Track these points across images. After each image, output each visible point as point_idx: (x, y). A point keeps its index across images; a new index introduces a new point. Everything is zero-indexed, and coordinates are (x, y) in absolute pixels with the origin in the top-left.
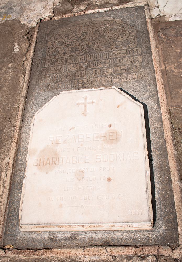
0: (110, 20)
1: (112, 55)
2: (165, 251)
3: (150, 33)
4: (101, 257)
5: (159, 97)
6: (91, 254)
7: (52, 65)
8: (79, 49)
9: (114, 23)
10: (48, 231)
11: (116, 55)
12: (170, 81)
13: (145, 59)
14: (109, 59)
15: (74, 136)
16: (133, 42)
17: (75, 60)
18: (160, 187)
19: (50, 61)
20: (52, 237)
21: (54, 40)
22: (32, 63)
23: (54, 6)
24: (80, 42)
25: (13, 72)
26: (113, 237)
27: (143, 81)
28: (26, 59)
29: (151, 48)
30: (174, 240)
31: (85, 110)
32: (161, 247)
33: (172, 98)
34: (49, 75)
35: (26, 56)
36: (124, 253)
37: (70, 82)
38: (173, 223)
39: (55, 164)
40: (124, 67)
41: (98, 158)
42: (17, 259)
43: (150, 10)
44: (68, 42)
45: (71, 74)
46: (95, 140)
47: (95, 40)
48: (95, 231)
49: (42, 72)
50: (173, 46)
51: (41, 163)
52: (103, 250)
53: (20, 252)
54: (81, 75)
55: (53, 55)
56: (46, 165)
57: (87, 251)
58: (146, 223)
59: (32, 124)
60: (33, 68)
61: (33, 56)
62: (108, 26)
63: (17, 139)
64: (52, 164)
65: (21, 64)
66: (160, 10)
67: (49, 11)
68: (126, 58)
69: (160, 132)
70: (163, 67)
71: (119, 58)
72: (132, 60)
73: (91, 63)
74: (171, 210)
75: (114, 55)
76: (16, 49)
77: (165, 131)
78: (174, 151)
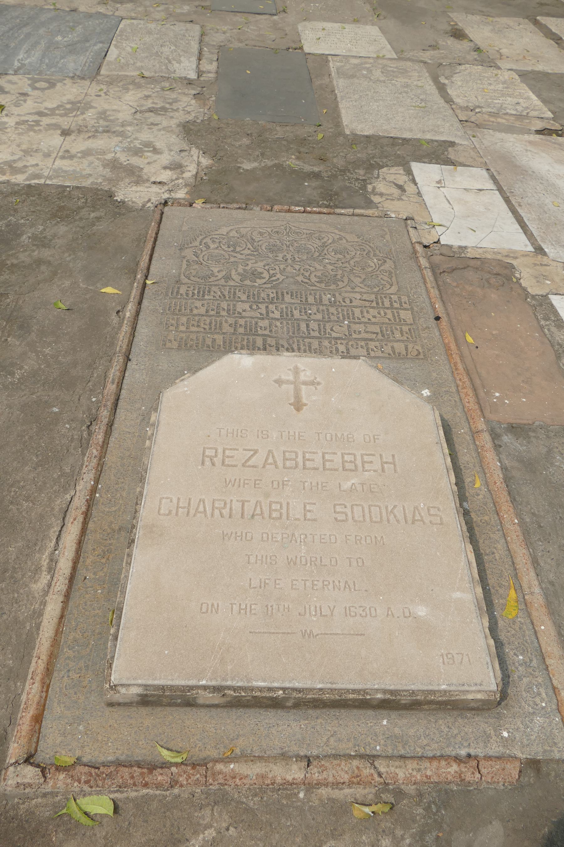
69: (240, 167)
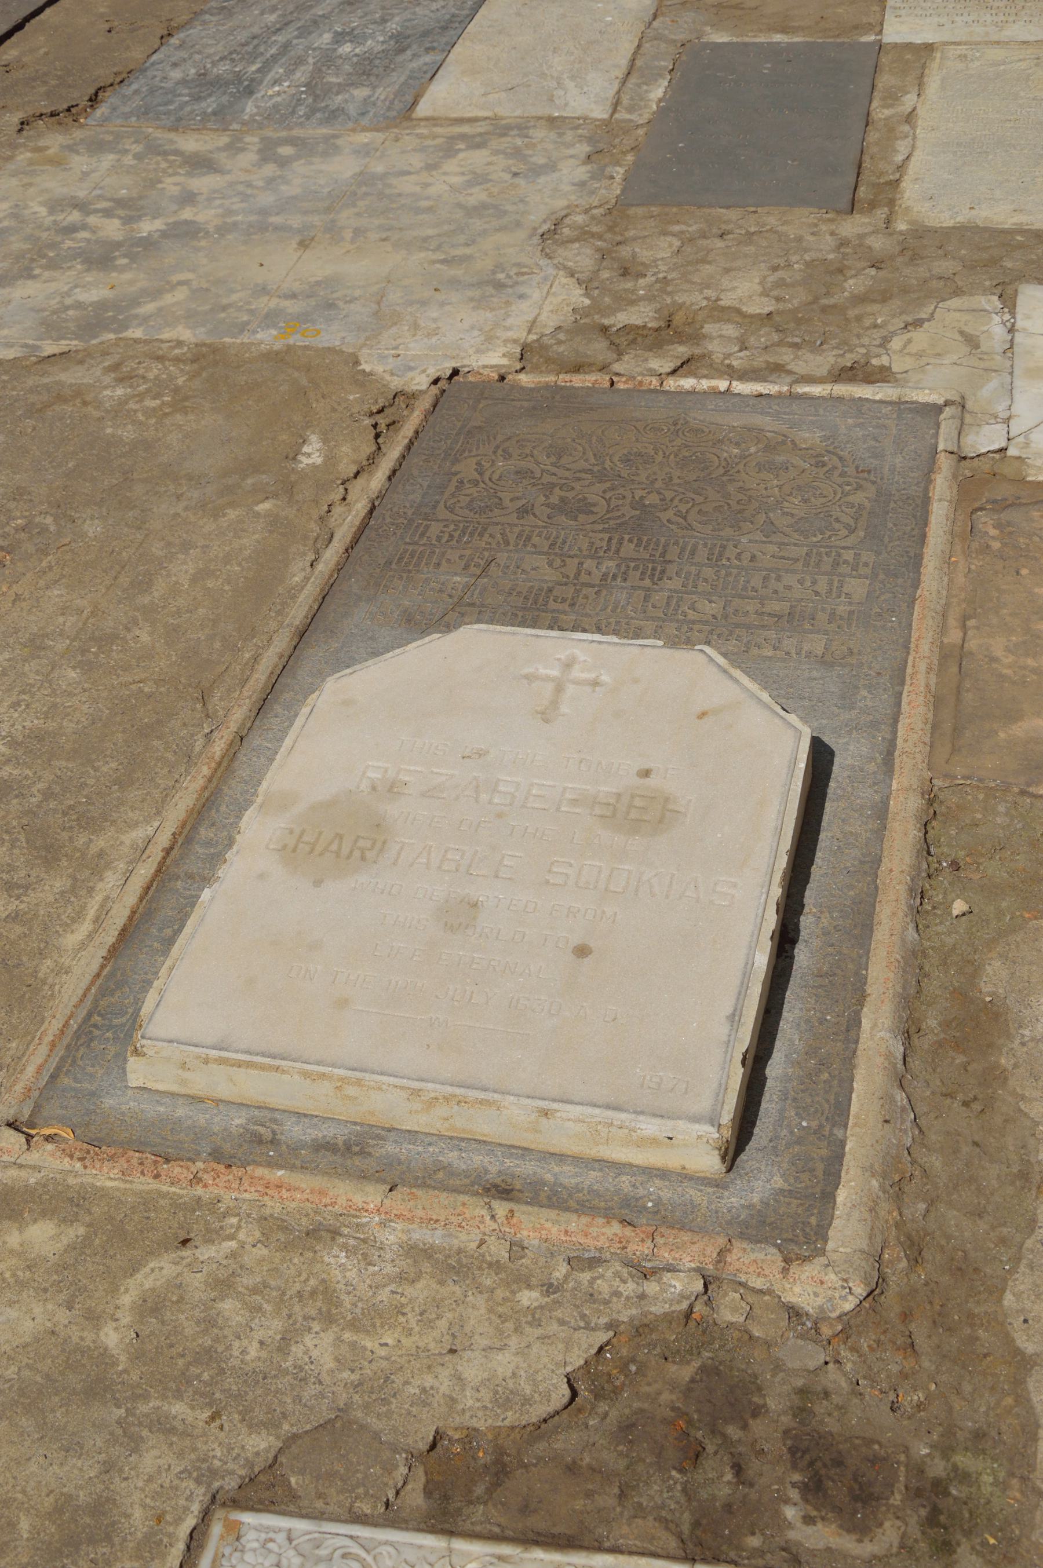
0: (767, 429)
1: (739, 554)
2: (755, 1261)
3: (935, 505)
4: (457, 1238)
5: (899, 734)
6: (420, 1213)
7: (454, 542)
8: (595, 509)
9: (783, 443)
10: (248, 1106)
11: (753, 558)
12: (968, 691)
13: (882, 593)
14: (718, 566)
15: (475, 778)
16: (847, 526)
17: (564, 542)
18: (800, 1040)
19: (452, 527)
20: (261, 1130)
21: (493, 457)
22: (364, 518)
23: (529, 332)
24: (608, 485)
25: (271, 532)
26: (535, 1173)
27: (846, 670)
28: (344, 499)
29: (922, 559)
30: (806, 1235)
31: (555, 703)
32: (739, 1245)
33: (955, 750)
34: (428, 572)
35: (346, 490)
36: (568, 1238)
37: (516, 615)
38: (819, 1173)
39: (363, 858)
40: (775, 606)
41: (557, 873)
42: (71, 1181)
43: (966, 427)
44: (555, 475)
45: (532, 587)
46: (563, 809)
47: (676, 488)
48: (462, 1139)
49: (401, 559)
50: (1024, 572)
51: (301, 845)
52: (475, 1208)
53: (97, 1154)
54: (573, 598)
55: (469, 506)
56: (321, 854)
57: (403, 1200)
58: (697, 1126)
59: (305, 710)
60: (363, 538)
61: (381, 496)
62: (753, 450)
63: (213, 765)
64: (349, 856)
65: (315, 514)
66: (1011, 435)
67: (503, 350)
68: (799, 576)
70: (954, 636)
71: (766, 569)
72: (822, 585)
73: (632, 565)
74: (828, 1128)
75: (747, 556)
76: (309, 455)
77: (885, 853)
78: (905, 929)
